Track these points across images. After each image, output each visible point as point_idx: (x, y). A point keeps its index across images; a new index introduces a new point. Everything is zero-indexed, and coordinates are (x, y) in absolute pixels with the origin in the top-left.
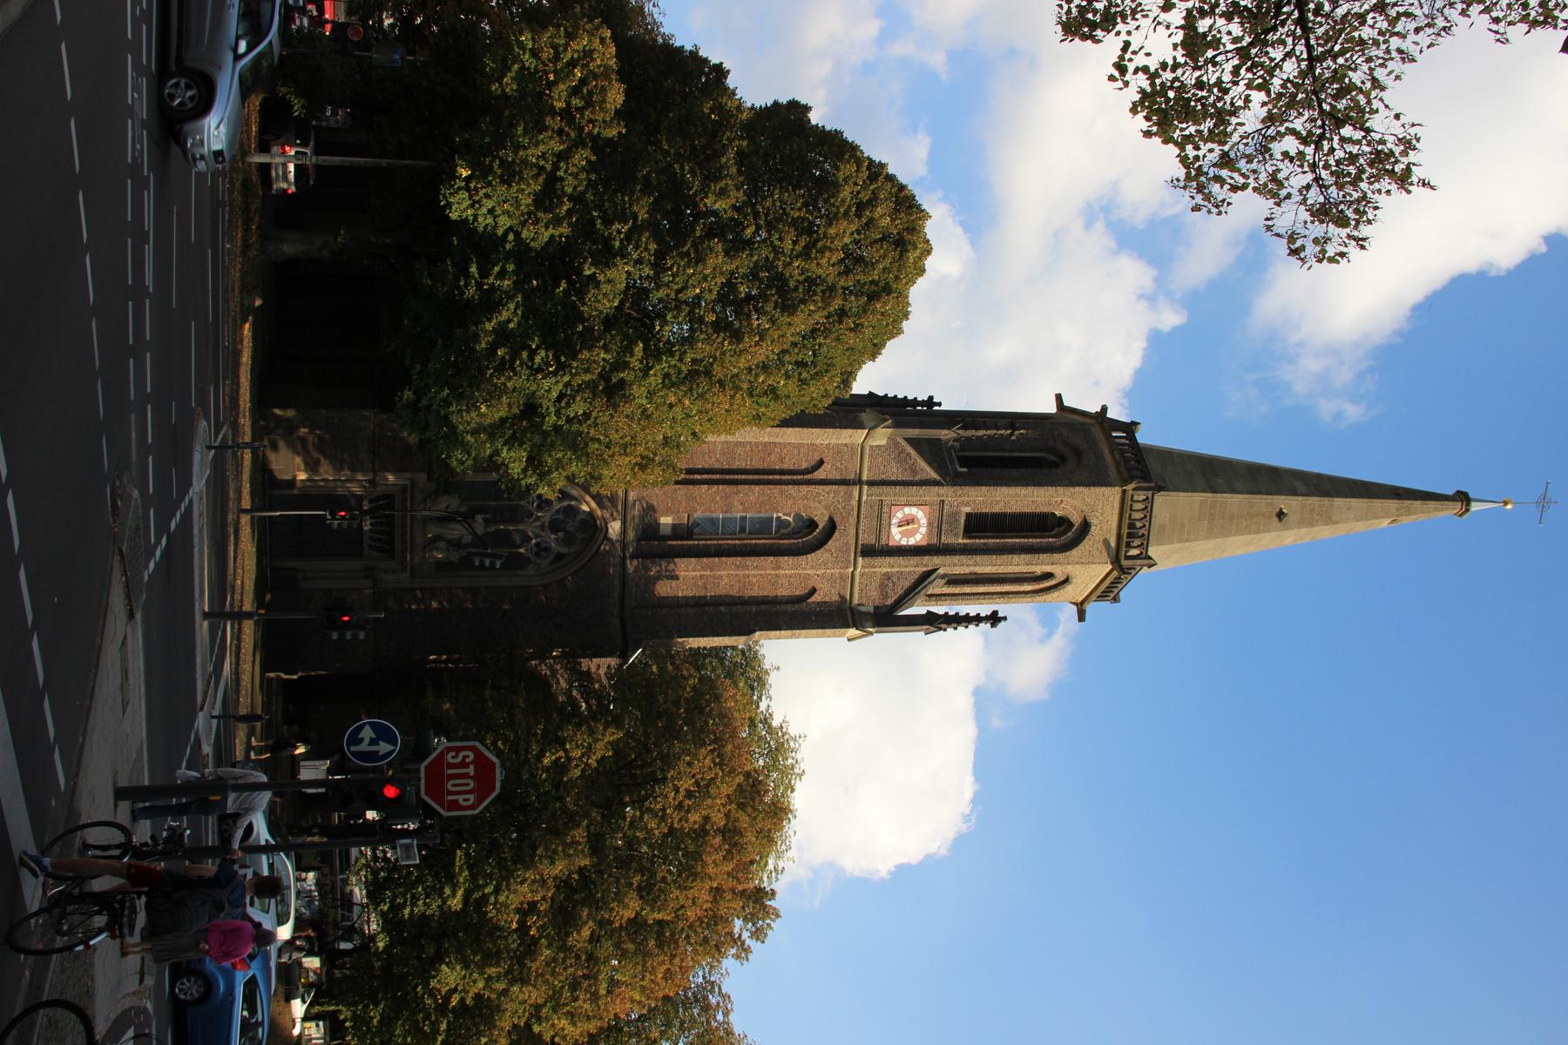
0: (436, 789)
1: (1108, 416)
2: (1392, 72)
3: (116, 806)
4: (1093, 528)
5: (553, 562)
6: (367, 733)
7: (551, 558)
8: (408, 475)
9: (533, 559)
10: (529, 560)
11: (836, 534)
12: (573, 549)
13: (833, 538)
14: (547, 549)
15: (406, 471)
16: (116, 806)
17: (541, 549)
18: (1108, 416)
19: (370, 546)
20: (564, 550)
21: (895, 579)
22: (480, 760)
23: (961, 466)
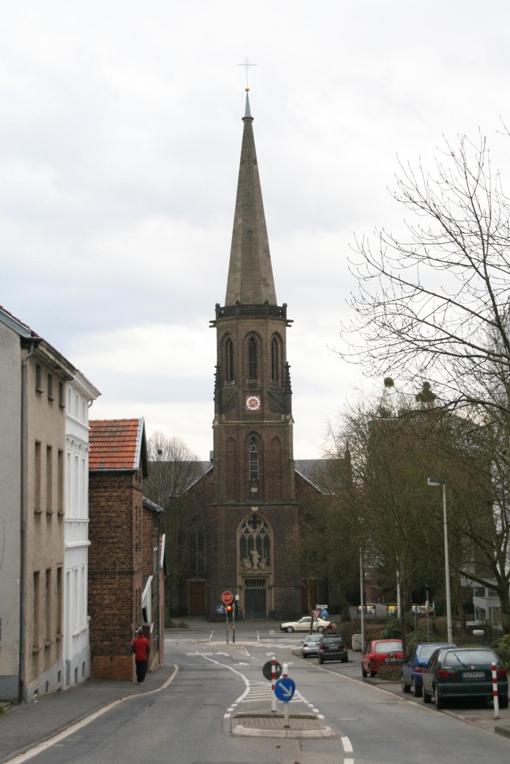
0: (229, 600)
1: (221, 307)
2: (78, 454)
3: (351, 662)
4: (253, 330)
5: (267, 527)
6: (219, 610)
7: (265, 528)
8: (238, 576)
9: (265, 534)
10: (266, 536)
11: (256, 431)
12: (262, 521)
13: (257, 432)
14: (263, 530)
15: (236, 577)
16: (351, 662)
17: (263, 531)
18: (221, 307)
19: (263, 587)
20: (263, 524)
21: (272, 407)
22: (225, 594)
23: (232, 382)
